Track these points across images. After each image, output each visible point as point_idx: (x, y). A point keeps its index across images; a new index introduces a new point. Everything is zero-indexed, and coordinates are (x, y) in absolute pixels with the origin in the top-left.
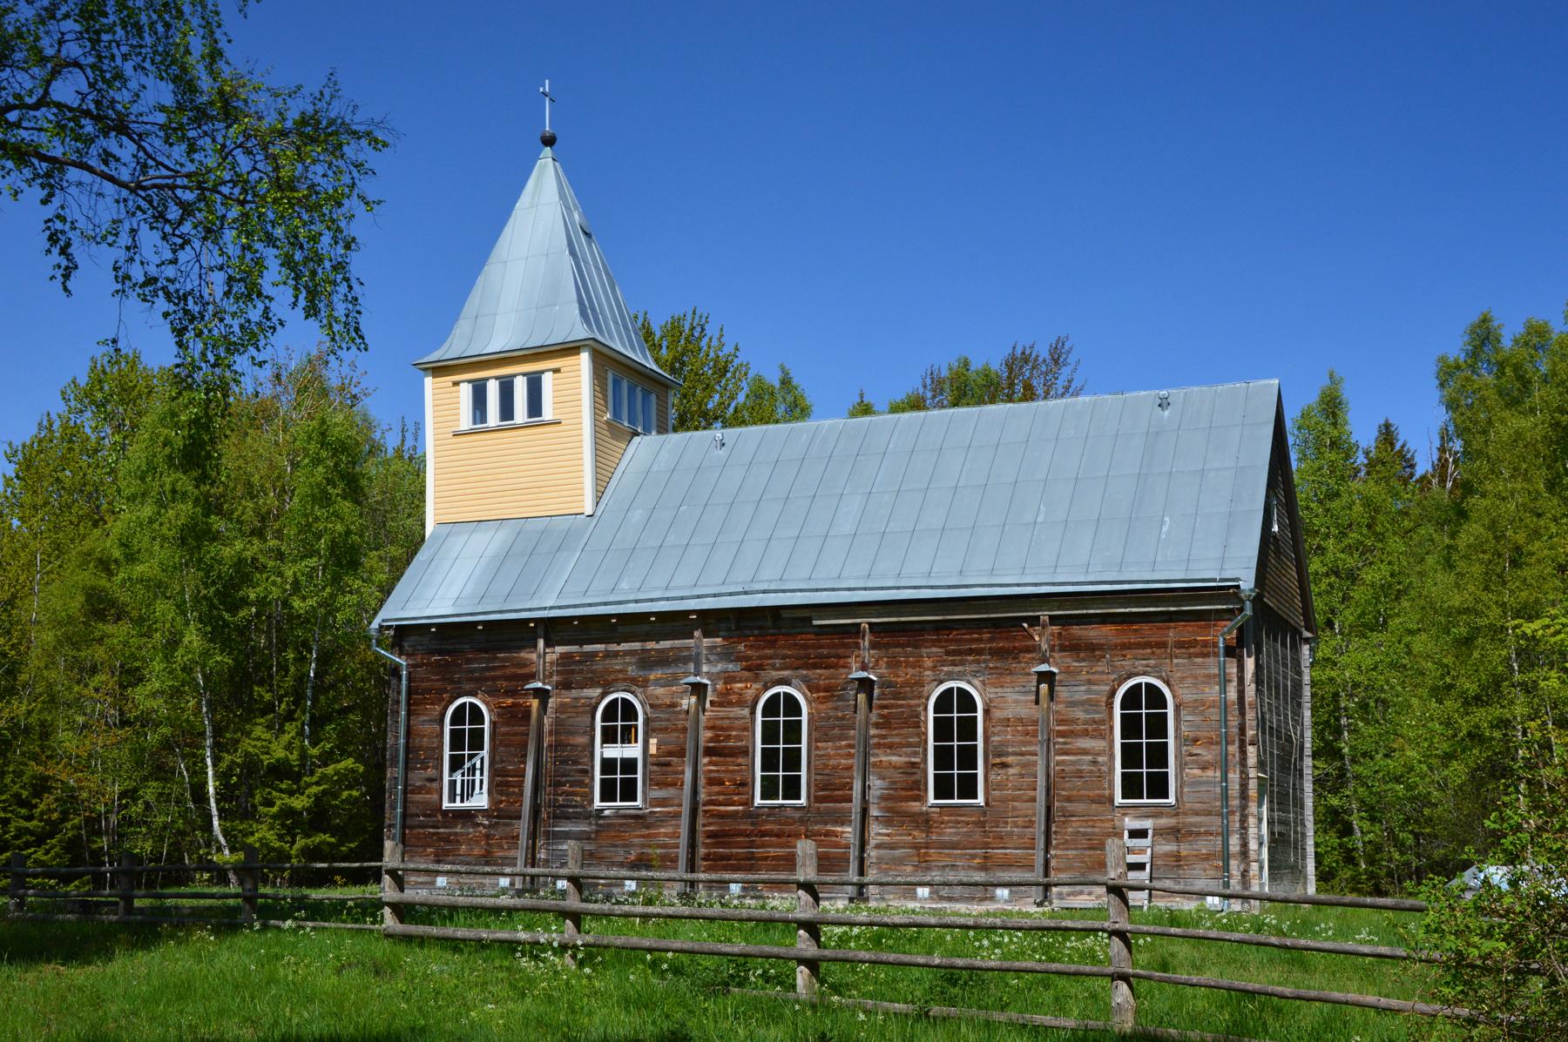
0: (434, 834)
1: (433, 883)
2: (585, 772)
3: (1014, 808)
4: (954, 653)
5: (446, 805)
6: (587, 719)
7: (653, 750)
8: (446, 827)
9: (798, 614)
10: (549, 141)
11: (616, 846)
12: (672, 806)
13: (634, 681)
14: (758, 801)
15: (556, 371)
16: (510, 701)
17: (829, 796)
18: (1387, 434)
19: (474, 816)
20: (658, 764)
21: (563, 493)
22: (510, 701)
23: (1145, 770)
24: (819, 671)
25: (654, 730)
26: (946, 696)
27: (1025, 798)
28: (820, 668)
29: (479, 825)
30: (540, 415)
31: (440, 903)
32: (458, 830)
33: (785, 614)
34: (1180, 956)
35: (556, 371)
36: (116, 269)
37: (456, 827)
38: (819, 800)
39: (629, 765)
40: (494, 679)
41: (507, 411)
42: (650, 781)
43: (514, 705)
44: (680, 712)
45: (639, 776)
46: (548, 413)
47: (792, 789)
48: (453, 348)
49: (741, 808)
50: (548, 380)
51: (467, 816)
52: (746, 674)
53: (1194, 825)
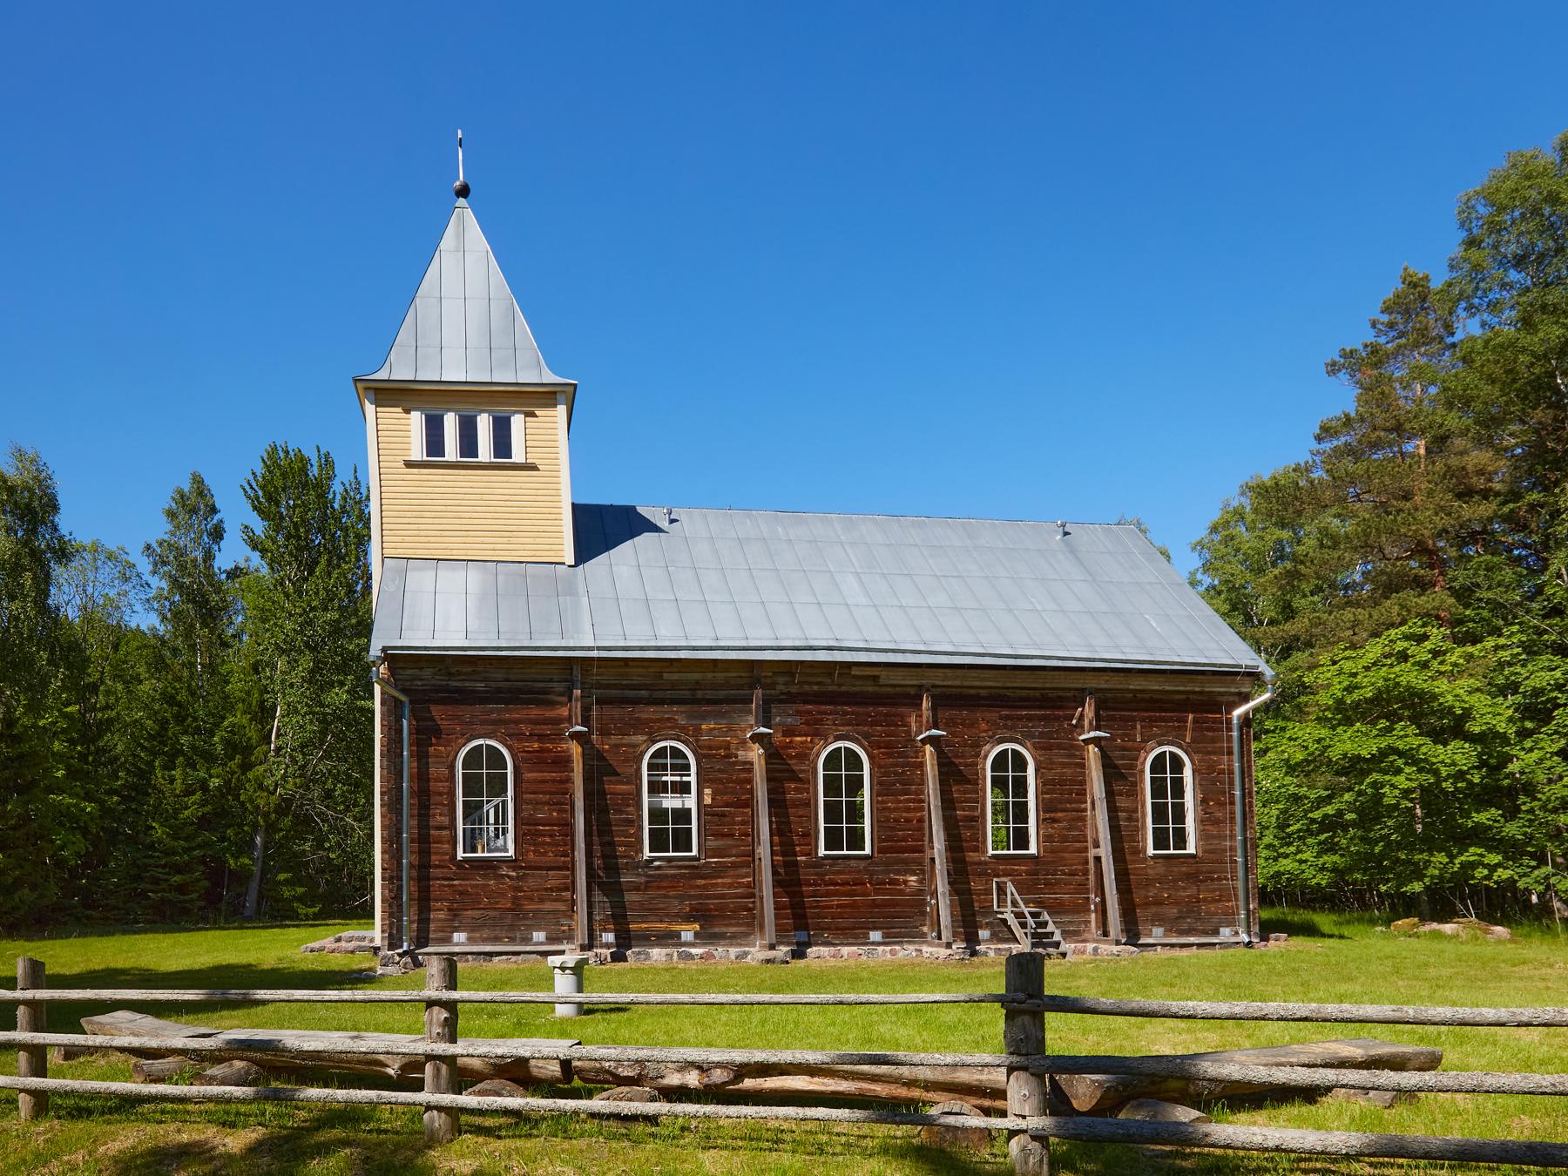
2: (630, 823)
3: (1063, 858)
4: (1007, 717)
7: (708, 800)
10: (463, 192)
11: (669, 897)
12: (730, 856)
13: (683, 728)
14: (822, 852)
17: (891, 847)
19: (496, 868)
21: (538, 540)
23: (844, 825)
26: (1002, 756)
27: (1071, 849)
30: (511, 458)
33: (855, 672)
39: (682, 815)
40: (517, 722)
43: (541, 750)
45: (694, 826)
46: (518, 456)
47: (856, 840)
48: (399, 369)
50: (517, 422)
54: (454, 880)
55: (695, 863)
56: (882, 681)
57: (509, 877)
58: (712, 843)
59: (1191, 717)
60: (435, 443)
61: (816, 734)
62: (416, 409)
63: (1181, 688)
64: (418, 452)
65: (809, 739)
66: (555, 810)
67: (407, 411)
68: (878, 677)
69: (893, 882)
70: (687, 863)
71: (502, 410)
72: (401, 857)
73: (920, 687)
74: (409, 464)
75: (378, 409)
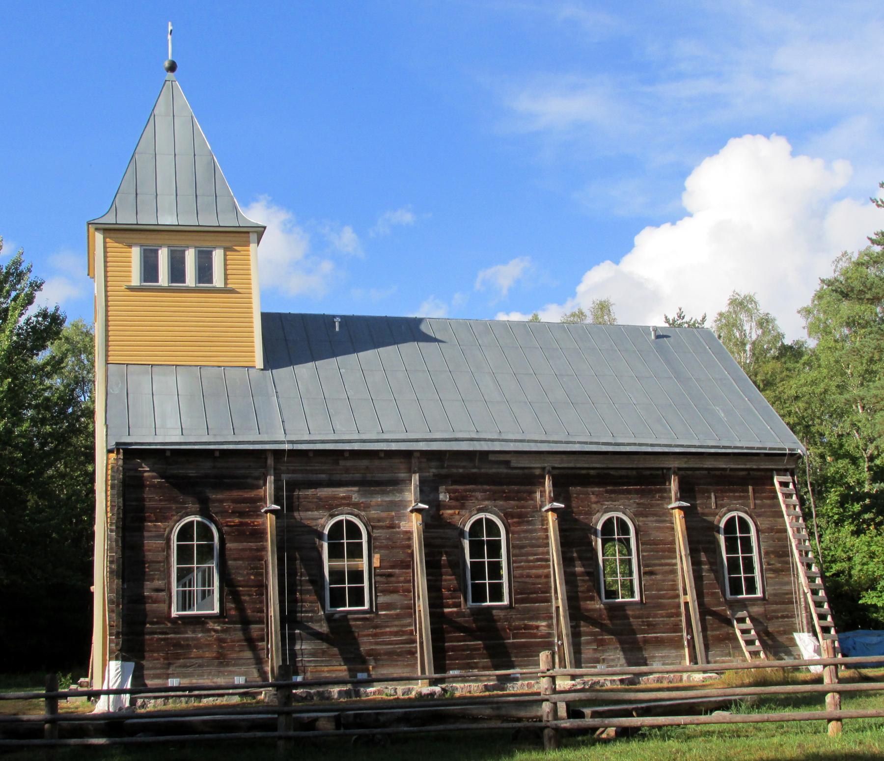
0: (162, 639)
5: (174, 613)
6: (376, 533)
7: (376, 563)
8: (175, 633)
9: (502, 458)
10: (172, 68)
13: (356, 505)
16: (237, 520)
20: (381, 575)
22: (237, 520)
23: (347, 585)
25: (375, 547)
28: (513, 500)
29: (209, 630)
31: (528, 716)
32: (190, 635)
33: (492, 458)
37: (186, 633)
38: (518, 601)
41: (177, 273)
42: (376, 590)
44: (398, 533)
45: (366, 584)
46: (218, 281)
47: (497, 594)
49: (455, 609)
50: (218, 256)
51: (198, 621)
52: (454, 503)
53: (774, 611)
54: (168, 634)
55: (368, 616)
57: (216, 631)
62: (136, 245)
66: (252, 574)
67: (130, 246)
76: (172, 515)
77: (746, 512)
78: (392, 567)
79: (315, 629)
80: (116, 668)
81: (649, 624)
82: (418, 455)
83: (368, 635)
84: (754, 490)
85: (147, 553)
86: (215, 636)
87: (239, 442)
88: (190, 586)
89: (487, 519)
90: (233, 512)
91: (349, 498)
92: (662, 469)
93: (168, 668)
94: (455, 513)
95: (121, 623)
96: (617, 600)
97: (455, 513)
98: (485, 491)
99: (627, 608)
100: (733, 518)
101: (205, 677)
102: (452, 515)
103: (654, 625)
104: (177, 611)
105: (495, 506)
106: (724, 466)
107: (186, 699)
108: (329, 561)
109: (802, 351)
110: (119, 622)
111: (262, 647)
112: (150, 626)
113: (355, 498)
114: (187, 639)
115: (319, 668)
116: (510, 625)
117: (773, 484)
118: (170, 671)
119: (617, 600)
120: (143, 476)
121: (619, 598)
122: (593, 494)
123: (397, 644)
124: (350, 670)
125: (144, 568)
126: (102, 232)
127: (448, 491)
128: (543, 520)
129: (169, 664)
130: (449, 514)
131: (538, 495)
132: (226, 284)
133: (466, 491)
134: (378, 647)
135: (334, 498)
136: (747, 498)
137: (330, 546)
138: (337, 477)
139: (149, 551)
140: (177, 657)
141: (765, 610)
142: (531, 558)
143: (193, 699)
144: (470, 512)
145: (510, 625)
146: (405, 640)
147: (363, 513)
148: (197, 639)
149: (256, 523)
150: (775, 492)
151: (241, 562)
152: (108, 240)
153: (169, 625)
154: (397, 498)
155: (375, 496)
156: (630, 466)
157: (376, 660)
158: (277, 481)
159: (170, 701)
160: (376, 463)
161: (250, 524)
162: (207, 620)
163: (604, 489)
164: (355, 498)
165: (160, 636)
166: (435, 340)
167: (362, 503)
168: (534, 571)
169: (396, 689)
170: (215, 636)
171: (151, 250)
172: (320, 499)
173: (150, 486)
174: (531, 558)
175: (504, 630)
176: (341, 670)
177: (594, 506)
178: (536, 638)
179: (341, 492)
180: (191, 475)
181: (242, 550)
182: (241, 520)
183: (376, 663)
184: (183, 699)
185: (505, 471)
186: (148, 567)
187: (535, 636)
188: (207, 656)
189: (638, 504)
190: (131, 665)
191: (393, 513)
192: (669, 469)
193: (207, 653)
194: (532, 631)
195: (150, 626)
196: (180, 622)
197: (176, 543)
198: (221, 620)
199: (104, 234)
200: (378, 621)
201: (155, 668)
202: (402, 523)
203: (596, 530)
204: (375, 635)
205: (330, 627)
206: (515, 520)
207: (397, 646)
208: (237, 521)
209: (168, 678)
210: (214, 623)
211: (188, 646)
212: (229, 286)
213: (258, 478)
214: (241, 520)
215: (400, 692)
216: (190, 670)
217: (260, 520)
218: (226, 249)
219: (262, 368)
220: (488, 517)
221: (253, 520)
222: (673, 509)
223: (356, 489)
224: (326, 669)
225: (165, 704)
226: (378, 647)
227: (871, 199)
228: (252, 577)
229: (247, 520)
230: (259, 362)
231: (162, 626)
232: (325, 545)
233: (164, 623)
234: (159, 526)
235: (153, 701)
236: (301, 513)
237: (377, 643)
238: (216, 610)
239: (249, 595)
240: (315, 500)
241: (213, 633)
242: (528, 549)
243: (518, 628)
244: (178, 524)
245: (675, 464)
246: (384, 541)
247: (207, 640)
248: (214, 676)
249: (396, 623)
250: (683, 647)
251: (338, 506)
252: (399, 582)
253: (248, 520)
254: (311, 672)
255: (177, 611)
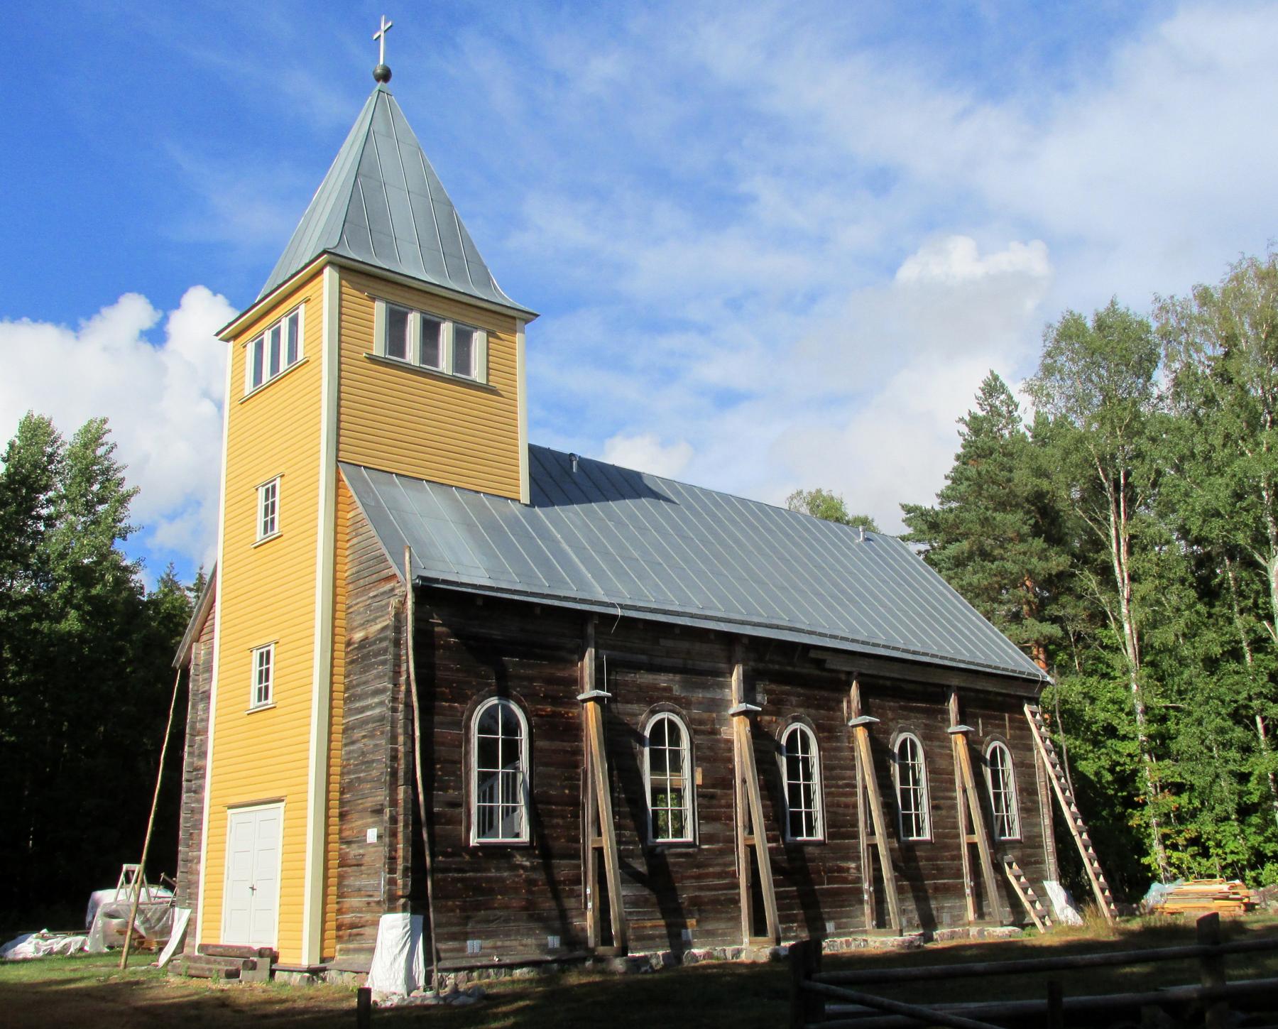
1: (463, 950)
5: (474, 840)
7: (699, 780)
13: (677, 700)
15: (307, 301)
18: (123, 479)
24: (822, 712)
28: (823, 709)
32: (493, 874)
33: (812, 654)
34: (998, 519)
35: (307, 301)
36: (933, 564)
37: (488, 870)
40: (531, 679)
43: (554, 715)
50: (478, 338)
54: (465, 872)
55: (690, 850)
56: (828, 666)
57: (523, 867)
58: (707, 829)
59: (1007, 715)
60: (396, 341)
61: (778, 713)
62: (381, 299)
63: (1004, 691)
64: (379, 349)
65: (774, 718)
66: (565, 787)
67: (373, 299)
68: (824, 661)
69: (841, 870)
70: (683, 850)
71: (435, 310)
72: (555, 805)
73: (849, 673)
74: (373, 359)
75: (491, 339)
76: (473, 694)
77: (1004, 742)
78: (714, 786)
79: (634, 868)
80: (404, 925)
81: (939, 869)
82: (745, 641)
83: (692, 877)
84: (1009, 718)
85: (436, 748)
86: (524, 876)
87: (564, 597)
88: (491, 801)
89: (669, 720)
90: (545, 697)
91: (669, 689)
92: (942, 686)
93: (466, 925)
94: (772, 720)
95: (410, 853)
96: (911, 838)
97: (772, 720)
98: (799, 695)
99: (916, 848)
100: (662, 721)
101: (512, 938)
102: (771, 722)
103: (942, 869)
104: (479, 837)
105: (809, 716)
106: (990, 689)
107: (496, 970)
108: (651, 775)
109: (1246, 570)
110: (408, 851)
111: (578, 892)
112: (443, 859)
113: (677, 690)
114: (489, 880)
115: (641, 924)
116: (824, 866)
117: (1023, 713)
118: (469, 928)
119: (911, 838)
120: (433, 631)
121: (913, 836)
122: (890, 709)
123: (721, 889)
124: (668, 926)
125: (434, 769)
126: (337, 269)
127: (767, 692)
128: (849, 737)
129: (468, 918)
130: (766, 721)
131: (845, 705)
132: (488, 380)
133: (783, 693)
134: (702, 894)
135: (655, 688)
136: (1004, 726)
137: (652, 751)
138: (657, 661)
139: (443, 744)
140: (477, 907)
141: (1023, 855)
142: (840, 783)
143: (503, 970)
144: (786, 720)
145: (824, 866)
146: (726, 884)
147: (684, 712)
148: (502, 880)
149: (570, 715)
150: (1026, 722)
151: (553, 769)
152: (344, 282)
153: (467, 858)
154: (717, 695)
155: (697, 690)
156: (913, 679)
157: (700, 911)
158: (598, 658)
159: (475, 974)
160: (698, 647)
161: (563, 715)
162: (515, 852)
163: (897, 705)
164: (677, 690)
165: (456, 875)
166: (667, 500)
167: (683, 698)
168: (843, 799)
169: (725, 950)
170: (524, 876)
171: (399, 312)
172: (640, 687)
173: (443, 647)
174: (840, 783)
175: (819, 872)
176: (656, 924)
177: (890, 724)
178: (846, 884)
179: (663, 680)
180: (494, 637)
181: (555, 751)
182: (554, 709)
183: (700, 915)
184: (491, 971)
185: (816, 672)
186: (440, 769)
187: (845, 881)
188: (515, 905)
189: (926, 725)
190: (420, 918)
191: (714, 715)
192: (949, 687)
193: (513, 901)
194: (843, 875)
195: (443, 859)
196: (480, 854)
197: (476, 735)
198: (531, 851)
199: (340, 273)
200: (700, 858)
201: (452, 925)
202: (723, 729)
203: (894, 753)
204: (699, 877)
205: (649, 865)
206: (826, 734)
207: (720, 892)
208: (549, 709)
209: (465, 940)
210: (523, 856)
211: (491, 892)
212: (490, 384)
213: (573, 652)
214: (554, 709)
215: (729, 955)
216: (493, 926)
217: (575, 711)
218: (491, 334)
219: (529, 503)
220: (671, 717)
221: (566, 710)
222: (853, 726)
223: (678, 677)
224: (649, 924)
225: (469, 980)
226: (702, 894)
227: (959, 432)
228: (567, 791)
229: (560, 709)
230: (525, 496)
231: (457, 859)
232: (647, 750)
233: (460, 856)
234: (456, 708)
235: (452, 975)
236: (619, 705)
237: (701, 888)
238: (525, 837)
239: (564, 817)
240: (635, 689)
241: (522, 872)
242: (838, 771)
243: (831, 870)
244: (479, 707)
245: (955, 682)
246: (705, 751)
247: (514, 881)
248: (523, 935)
249: (720, 861)
250: (963, 896)
251: (659, 699)
252: (721, 807)
253: (563, 710)
254: (634, 928)
255: (479, 837)
